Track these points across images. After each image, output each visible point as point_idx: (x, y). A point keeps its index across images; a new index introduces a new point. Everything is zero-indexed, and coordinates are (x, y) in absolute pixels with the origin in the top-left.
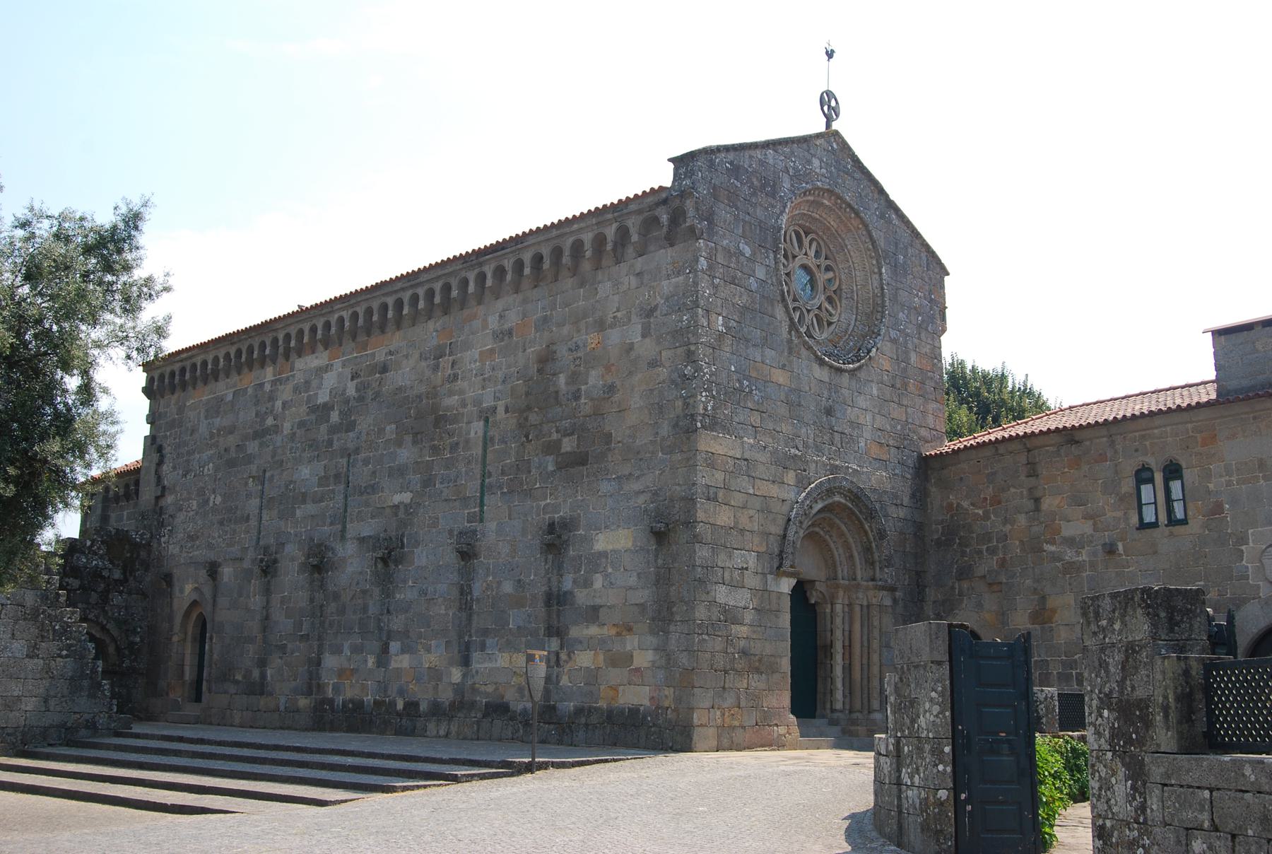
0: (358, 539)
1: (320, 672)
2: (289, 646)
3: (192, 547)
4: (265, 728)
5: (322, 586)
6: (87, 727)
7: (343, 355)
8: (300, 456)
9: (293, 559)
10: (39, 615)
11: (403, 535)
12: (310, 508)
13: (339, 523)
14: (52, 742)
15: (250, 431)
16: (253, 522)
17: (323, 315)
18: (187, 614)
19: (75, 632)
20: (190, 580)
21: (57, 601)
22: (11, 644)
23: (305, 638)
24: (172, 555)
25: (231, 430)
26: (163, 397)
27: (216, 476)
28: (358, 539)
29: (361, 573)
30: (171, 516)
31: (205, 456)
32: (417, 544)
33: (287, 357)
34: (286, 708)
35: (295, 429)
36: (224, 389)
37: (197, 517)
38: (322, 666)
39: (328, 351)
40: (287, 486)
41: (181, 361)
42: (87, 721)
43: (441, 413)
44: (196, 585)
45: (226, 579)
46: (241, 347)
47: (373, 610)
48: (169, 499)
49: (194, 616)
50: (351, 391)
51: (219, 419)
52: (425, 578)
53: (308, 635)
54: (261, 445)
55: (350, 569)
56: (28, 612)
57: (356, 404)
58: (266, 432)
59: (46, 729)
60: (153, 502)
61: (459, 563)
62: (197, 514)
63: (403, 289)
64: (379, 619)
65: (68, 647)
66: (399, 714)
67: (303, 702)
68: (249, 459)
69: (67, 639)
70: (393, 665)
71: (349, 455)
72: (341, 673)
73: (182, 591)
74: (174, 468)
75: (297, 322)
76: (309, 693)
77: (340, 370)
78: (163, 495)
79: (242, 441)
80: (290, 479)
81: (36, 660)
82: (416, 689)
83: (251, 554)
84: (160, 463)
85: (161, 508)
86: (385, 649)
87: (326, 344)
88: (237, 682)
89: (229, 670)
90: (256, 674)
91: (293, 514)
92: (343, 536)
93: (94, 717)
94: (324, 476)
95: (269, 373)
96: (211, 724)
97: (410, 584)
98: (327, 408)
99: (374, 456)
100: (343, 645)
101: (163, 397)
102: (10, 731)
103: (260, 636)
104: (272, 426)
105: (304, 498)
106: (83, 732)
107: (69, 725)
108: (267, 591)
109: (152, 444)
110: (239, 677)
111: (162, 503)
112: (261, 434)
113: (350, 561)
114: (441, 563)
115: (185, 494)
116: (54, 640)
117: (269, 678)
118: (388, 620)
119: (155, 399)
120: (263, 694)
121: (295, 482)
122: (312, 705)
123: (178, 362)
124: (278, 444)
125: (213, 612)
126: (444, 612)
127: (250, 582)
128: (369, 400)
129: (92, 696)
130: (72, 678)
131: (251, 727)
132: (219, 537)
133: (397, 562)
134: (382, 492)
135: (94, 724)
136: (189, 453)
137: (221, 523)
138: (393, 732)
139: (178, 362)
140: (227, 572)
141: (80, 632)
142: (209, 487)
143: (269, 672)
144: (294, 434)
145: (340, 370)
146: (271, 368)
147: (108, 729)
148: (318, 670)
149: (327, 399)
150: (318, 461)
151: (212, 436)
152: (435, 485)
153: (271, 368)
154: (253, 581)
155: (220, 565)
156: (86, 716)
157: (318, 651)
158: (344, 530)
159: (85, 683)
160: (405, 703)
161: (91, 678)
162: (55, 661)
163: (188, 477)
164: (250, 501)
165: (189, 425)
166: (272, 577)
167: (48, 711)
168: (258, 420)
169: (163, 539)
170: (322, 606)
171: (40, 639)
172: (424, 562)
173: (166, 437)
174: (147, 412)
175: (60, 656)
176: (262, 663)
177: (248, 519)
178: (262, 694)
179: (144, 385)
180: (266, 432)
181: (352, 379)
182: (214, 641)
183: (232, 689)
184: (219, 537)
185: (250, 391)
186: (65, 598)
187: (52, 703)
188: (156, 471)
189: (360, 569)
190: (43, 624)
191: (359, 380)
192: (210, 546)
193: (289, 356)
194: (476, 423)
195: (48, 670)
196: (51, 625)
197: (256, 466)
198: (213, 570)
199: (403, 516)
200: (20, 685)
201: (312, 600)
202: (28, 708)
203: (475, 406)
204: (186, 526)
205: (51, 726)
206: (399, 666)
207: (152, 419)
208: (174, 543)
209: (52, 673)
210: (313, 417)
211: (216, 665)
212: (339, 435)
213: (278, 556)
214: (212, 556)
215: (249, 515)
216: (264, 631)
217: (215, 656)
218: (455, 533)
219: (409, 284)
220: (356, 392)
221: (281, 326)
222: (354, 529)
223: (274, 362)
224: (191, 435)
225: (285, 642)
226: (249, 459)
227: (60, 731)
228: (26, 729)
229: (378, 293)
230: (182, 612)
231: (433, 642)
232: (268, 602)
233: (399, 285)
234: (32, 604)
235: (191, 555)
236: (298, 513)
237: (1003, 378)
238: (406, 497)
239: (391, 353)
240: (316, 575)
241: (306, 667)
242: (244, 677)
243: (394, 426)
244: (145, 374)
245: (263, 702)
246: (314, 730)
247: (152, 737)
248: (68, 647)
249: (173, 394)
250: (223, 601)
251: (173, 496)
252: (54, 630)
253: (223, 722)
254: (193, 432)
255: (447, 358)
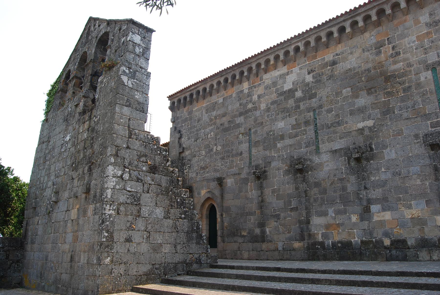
0: (331, 152)
1: (310, 227)
2: (282, 215)
3: (204, 172)
4: (268, 260)
5: (304, 180)
6: (197, 263)
7: (298, 65)
8: (275, 117)
9: (279, 169)
10: (169, 192)
11: (371, 144)
12: (288, 142)
13: (313, 145)
14: (180, 273)
15: (237, 113)
16: (246, 155)
17: (282, 48)
18: (203, 205)
19: (188, 203)
20: (204, 188)
21: (178, 184)
22: (155, 209)
23: (295, 209)
24: (192, 178)
25: (224, 115)
26: (179, 110)
27: (216, 137)
28: (331, 152)
29: (336, 169)
30: (189, 160)
31: (207, 130)
32: (385, 147)
33: (257, 75)
34: (283, 248)
35: (269, 106)
36: (217, 98)
37: (206, 159)
38: (311, 223)
39: (286, 66)
40: (268, 134)
41: (190, 91)
42: (196, 259)
43: (389, 74)
44: (209, 190)
45: (229, 185)
46: (228, 76)
47: (350, 188)
48: (187, 153)
49: (207, 205)
50: (309, 78)
51: (215, 112)
52: (397, 165)
53: (297, 208)
54: (245, 118)
55: (326, 169)
56: (163, 190)
57: (314, 85)
58: (247, 111)
59: (176, 264)
60: (178, 155)
61: (428, 153)
62: (205, 156)
63: (344, 21)
64: (358, 194)
65: (185, 213)
66: (386, 248)
67: (297, 245)
68: (238, 126)
69: (184, 208)
70: (376, 218)
71: (314, 110)
72: (328, 227)
73: (199, 193)
74: (189, 139)
75: (265, 56)
76: (302, 239)
77: (299, 71)
78: (183, 152)
79: (232, 118)
80: (270, 130)
81: (168, 220)
82: (402, 232)
83: (246, 170)
84: (180, 138)
85: (183, 157)
86: (367, 210)
87: (285, 63)
88: (244, 236)
89: (237, 230)
90: (258, 231)
91: (275, 146)
92: (317, 151)
93: (200, 256)
94: (296, 124)
95: (245, 85)
96: (226, 258)
97: (383, 170)
98: (291, 92)
99: (335, 107)
100: (328, 210)
101: (179, 110)
102: (157, 266)
103: (258, 212)
104: (252, 108)
105: (282, 137)
106: (195, 266)
107: (188, 261)
108: (261, 188)
109: (175, 130)
110: (244, 233)
111: (183, 155)
112: (245, 113)
113: (326, 164)
114: (410, 155)
115: (197, 149)
116: (177, 208)
117: (268, 233)
118: (367, 193)
119: (174, 111)
120: (265, 242)
121: (274, 131)
122: (305, 246)
123: (189, 91)
124: (258, 115)
125: (222, 202)
126: (420, 183)
127: (247, 184)
128: (325, 80)
129: (198, 243)
130: (187, 232)
131: (257, 260)
132: (222, 165)
133: (368, 160)
134: (346, 124)
135: (200, 260)
136: (197, 130)
137: (223, 158)
138: (385, 259)
139: (189, 91)
140: (229, 182)
141: (190, 204)
142: (212, 143)
143: (267, 230)
144: (269, 108)
145: (299, 71)
146: (247, 83)
147: (207, 263)
148: (308, 226)
149: (291, 86)
150: (289, 118)
151: (211, 120)
152: (394, 113)
153: (247, 83)
154: (249, 184)
155: (224, 178)
156: (196, 256)
157: (307, 216)
158: (318, 148)
159: (194, 235)
160: (391, 241)
161: (197, 232)
162: (178, 221)
163: (198, 141)
164: (242, 145)
165: (196, 118)
166: (263, 180)
167: (177, 253)
168: (242, 107)
169: (185, 171)
170: (306, 191)
171: (170, 207)
172: (393, 155)
173: (182, 126)
174: (171, 118)
175: (181, 218)
176: (262, 225)
177: (241, 154)
178: (263, 241)
179: (169, 106)
180: (247, 111)
181: (309, 73)
182: (224, 216)
183: (240, 240)
184: (222, 165)
185: (234, 95)
186: (181, 183)
187: (179, 247)
188: (179, 141)
189: (335, 168)
190: (171, 199)
191: (315, 73)
192: (216, 171)
193: (258, 75)
194: (424, 74)
195: (175, 227)
196: (175, 198)
197: (243, 128)
198: (220, 181)
199: (369, 133)
200: (161, 236)
201: (297, 189)
202: (166, 251)
203: (420, 64)
204: (199, 163)
205: (179, 263)
206: (382, 219)
207: (173, 121)
208: (192, 172)
209: (178, 229)
210: (282, 98)
211: (227, 228)
212: (304, 102)
213: (267, 169)
214: (218, 175)
215: (242, 152)
216: (261, 208)
217: (226, 224)
218: (421, 136)
219: (350, 16)
220: (313, 79)
221: (254, 60)
222: (324, 147)
223: (248, 78)
224: (198, 122)
225: (279, 213)
226: (238, 126)
227: (184, 266)
228: (166, 265)
229: (325, 27)
230: (200, 204)
231: (412, 202)
232: (262, 193)
233: (342, 19)
234: (165, 185)
235: (204, 176)
236: (279, 145)
237: (26, 251)
238: (370, 123)
239: (337, 55)
240: (299, 175)
241: (298, 225)
242: (249, 233)
243: (349, 89)
244: (169, 101)
245: (264, 246)
246: (310, 260)
247: (247, 268)
248: (185, 213)
249: (185, 107)
250: (227, 196)
251: (189, 151)
252: (177, 202)
253: (235, 257)
254: (199, 121)
255: (387, 46)
